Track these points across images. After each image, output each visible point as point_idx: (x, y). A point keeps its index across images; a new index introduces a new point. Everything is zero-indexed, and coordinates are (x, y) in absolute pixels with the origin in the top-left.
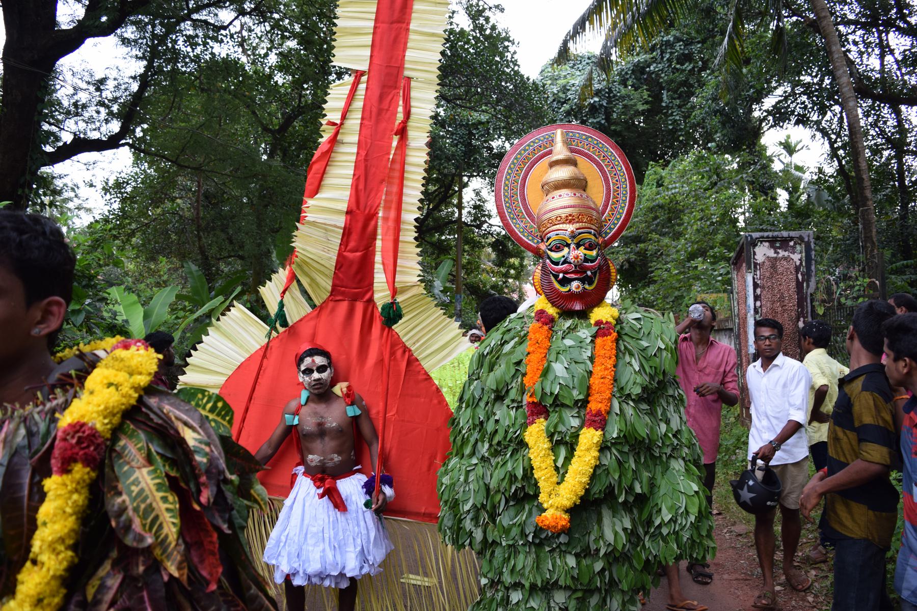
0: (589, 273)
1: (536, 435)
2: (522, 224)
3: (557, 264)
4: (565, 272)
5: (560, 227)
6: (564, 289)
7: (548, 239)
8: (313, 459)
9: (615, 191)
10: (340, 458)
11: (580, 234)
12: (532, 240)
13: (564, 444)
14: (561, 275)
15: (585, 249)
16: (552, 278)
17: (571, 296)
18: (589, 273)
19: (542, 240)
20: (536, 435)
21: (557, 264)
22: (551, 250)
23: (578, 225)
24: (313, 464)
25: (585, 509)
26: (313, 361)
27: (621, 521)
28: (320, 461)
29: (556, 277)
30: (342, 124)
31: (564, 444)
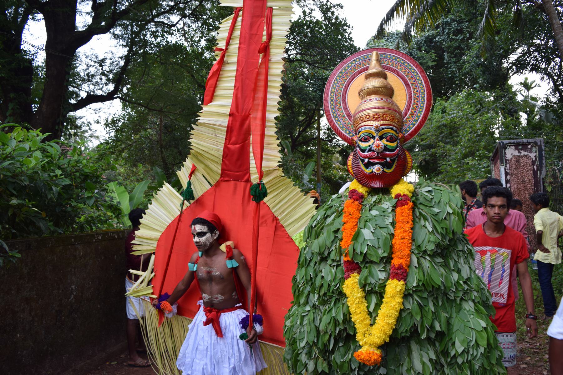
0: (388, 159)
1: (352, 286)
2: (342, 122)
4: (370, 158)
5: (361, 125)
6: (368, 171)
7: (359, 132)
9: (415, 99)
10: (223, 297)
11: (383, 129)
13: (374, 293)
14: (366, 160)
15: (387, 141)
16: (360, 162)
17: (373, 177)
18: (388, 159)
20: (352, 286)
21: (363, 151)
22: (361, 141)
25: (396, 344)
26: (195, 228)
27: (428, 354)
28: (209, 299)
29: (363, 161)
31: (374, 293)
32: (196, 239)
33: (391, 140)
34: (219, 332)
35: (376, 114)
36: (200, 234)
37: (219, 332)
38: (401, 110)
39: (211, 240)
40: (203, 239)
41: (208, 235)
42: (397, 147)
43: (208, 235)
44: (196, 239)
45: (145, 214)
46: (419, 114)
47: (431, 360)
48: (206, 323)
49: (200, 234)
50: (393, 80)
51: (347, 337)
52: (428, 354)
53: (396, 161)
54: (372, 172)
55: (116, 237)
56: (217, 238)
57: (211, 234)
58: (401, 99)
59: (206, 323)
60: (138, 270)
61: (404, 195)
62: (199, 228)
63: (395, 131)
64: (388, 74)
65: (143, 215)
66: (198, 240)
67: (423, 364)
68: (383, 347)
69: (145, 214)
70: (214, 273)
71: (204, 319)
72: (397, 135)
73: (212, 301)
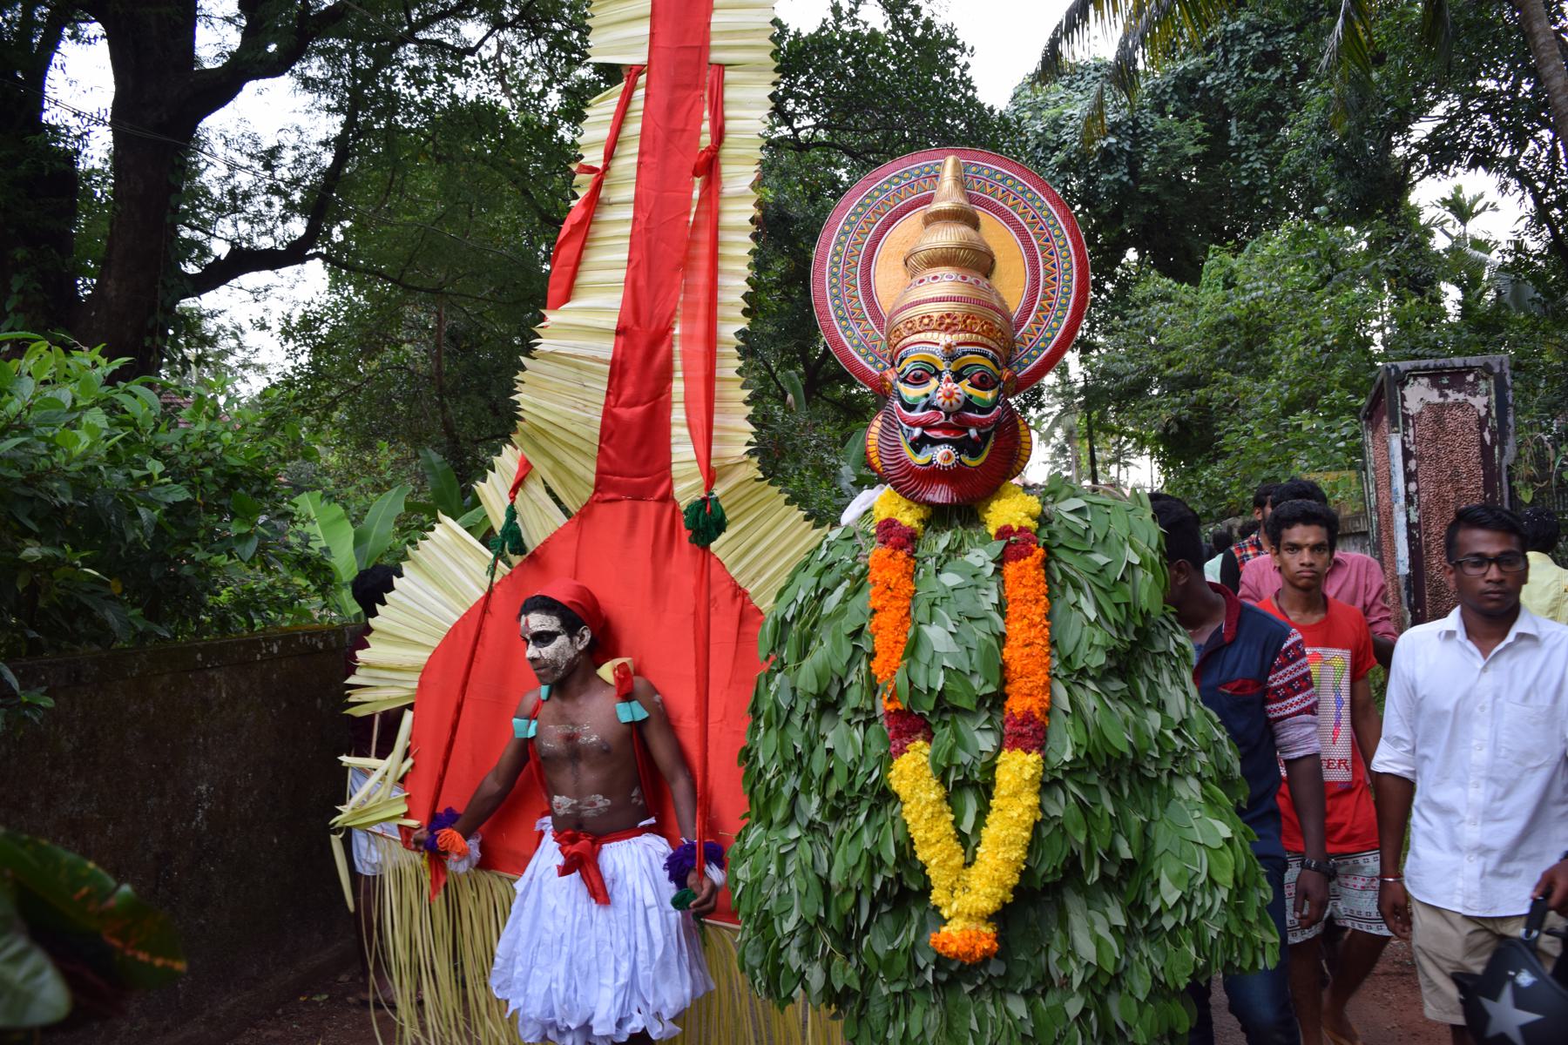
1: (912, 773)
3: (911, 408)
6: (920, 459)
7: (902, 360)
8: (562, 802)
12: (874, 364)
13: (968, 787)
14: (917, 432)
15: (973, 385)
18: (973, 433)
19: (893, 365)
21: (911, 408)
22: (904, 381)
23: (962, 337)
24: (561, 812)
25: (1029, 906)
27: (1105, 915)
28: (572, 807)
30: (606, 168)
31: (968, 787)
32: (532, 651)
33: (982, 384)
34: (599, 892)
35: (949, 316)
36: (543, 638)
37: (599, 892)
38: (1012, 309)
39: (571, 654)
40: (548, 651)
41: (562, 640)
42: (997, 403)
43: (562, 640)
44: (532, 651)
45: (384, 603)
46: (1055, 325)
47: (1114, 929)
48: (565, 871)
49: (543, 638)
50: (996, 235)
51: (906, 891)
52: (1105, 915)
53: (992, 440)
54: (931, 462)
55: (320, 645)
56: (587, 648)
57: (571, 637)
58: (1011, 284)
59: (565, 871)
60: (367, 755)
61: (1021, 529)
62: (537, 621)
63: (993, 360)
64: (984, 216)
65: (378, 607)
66: (536, 655)
67: (1098, 941)
68: (1002, 917)
69: (384, 603)
70: (583, 740)
71: (560, 860)
72: (998, 373)
73: (580, 811)
